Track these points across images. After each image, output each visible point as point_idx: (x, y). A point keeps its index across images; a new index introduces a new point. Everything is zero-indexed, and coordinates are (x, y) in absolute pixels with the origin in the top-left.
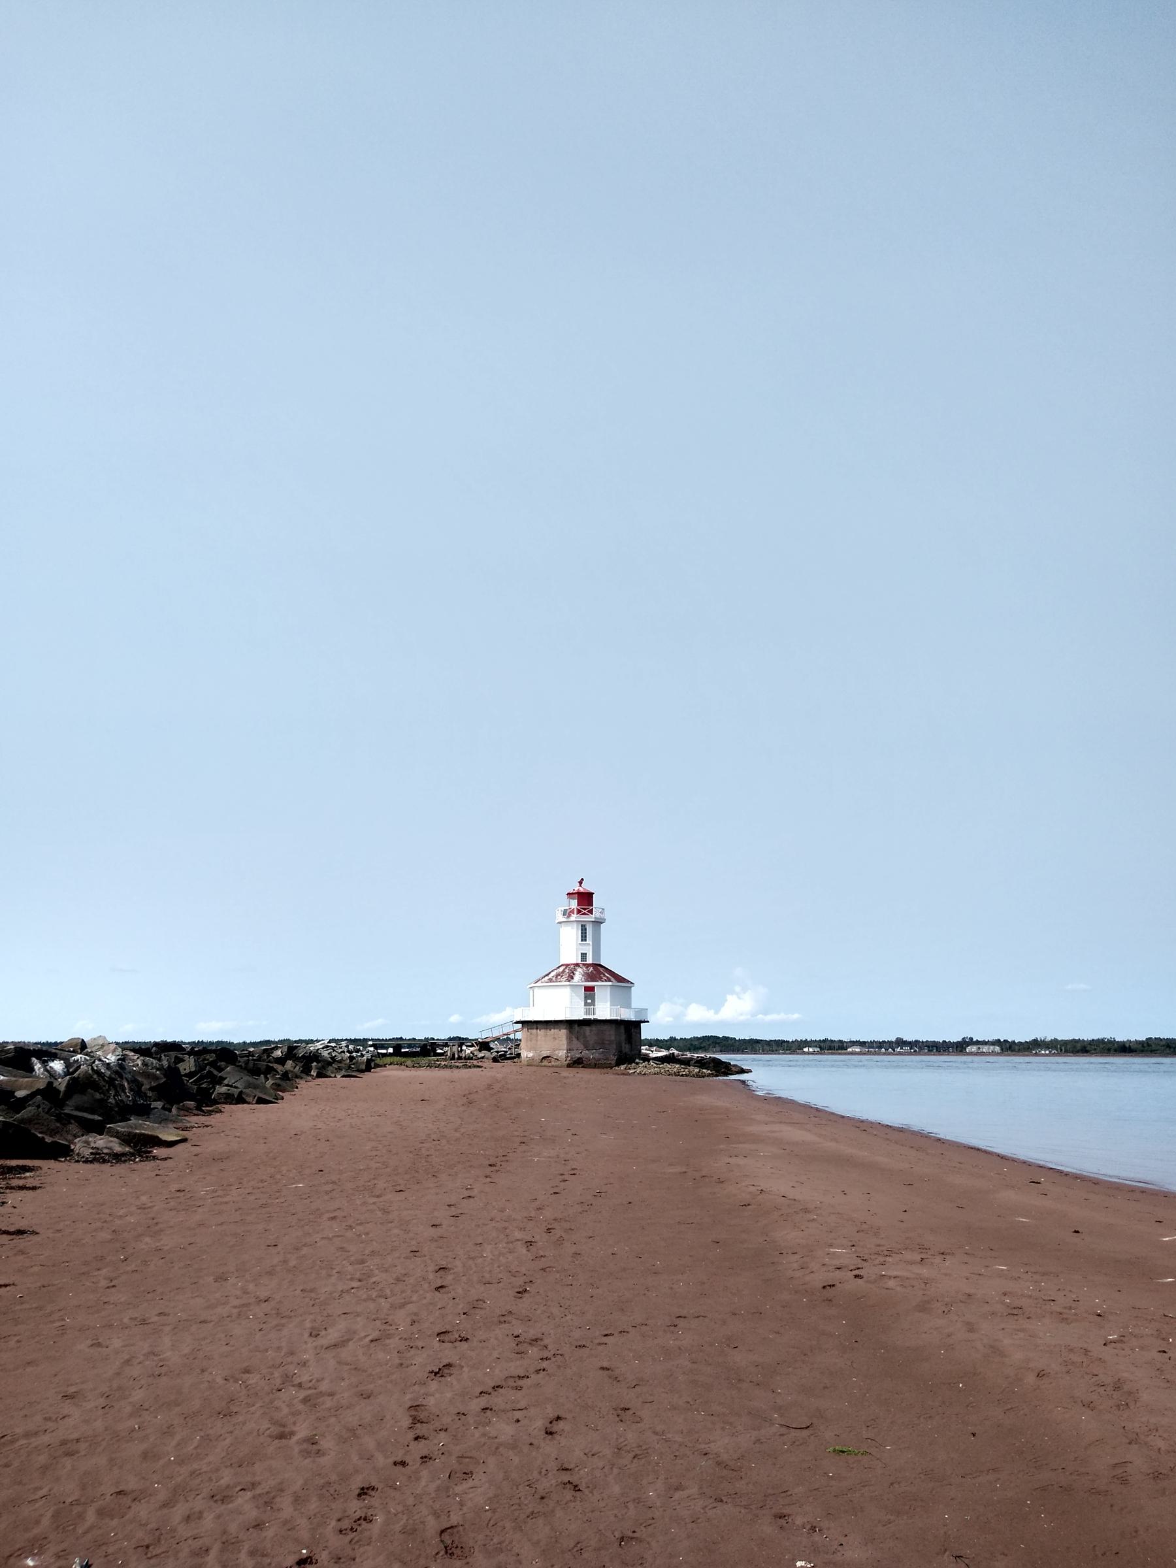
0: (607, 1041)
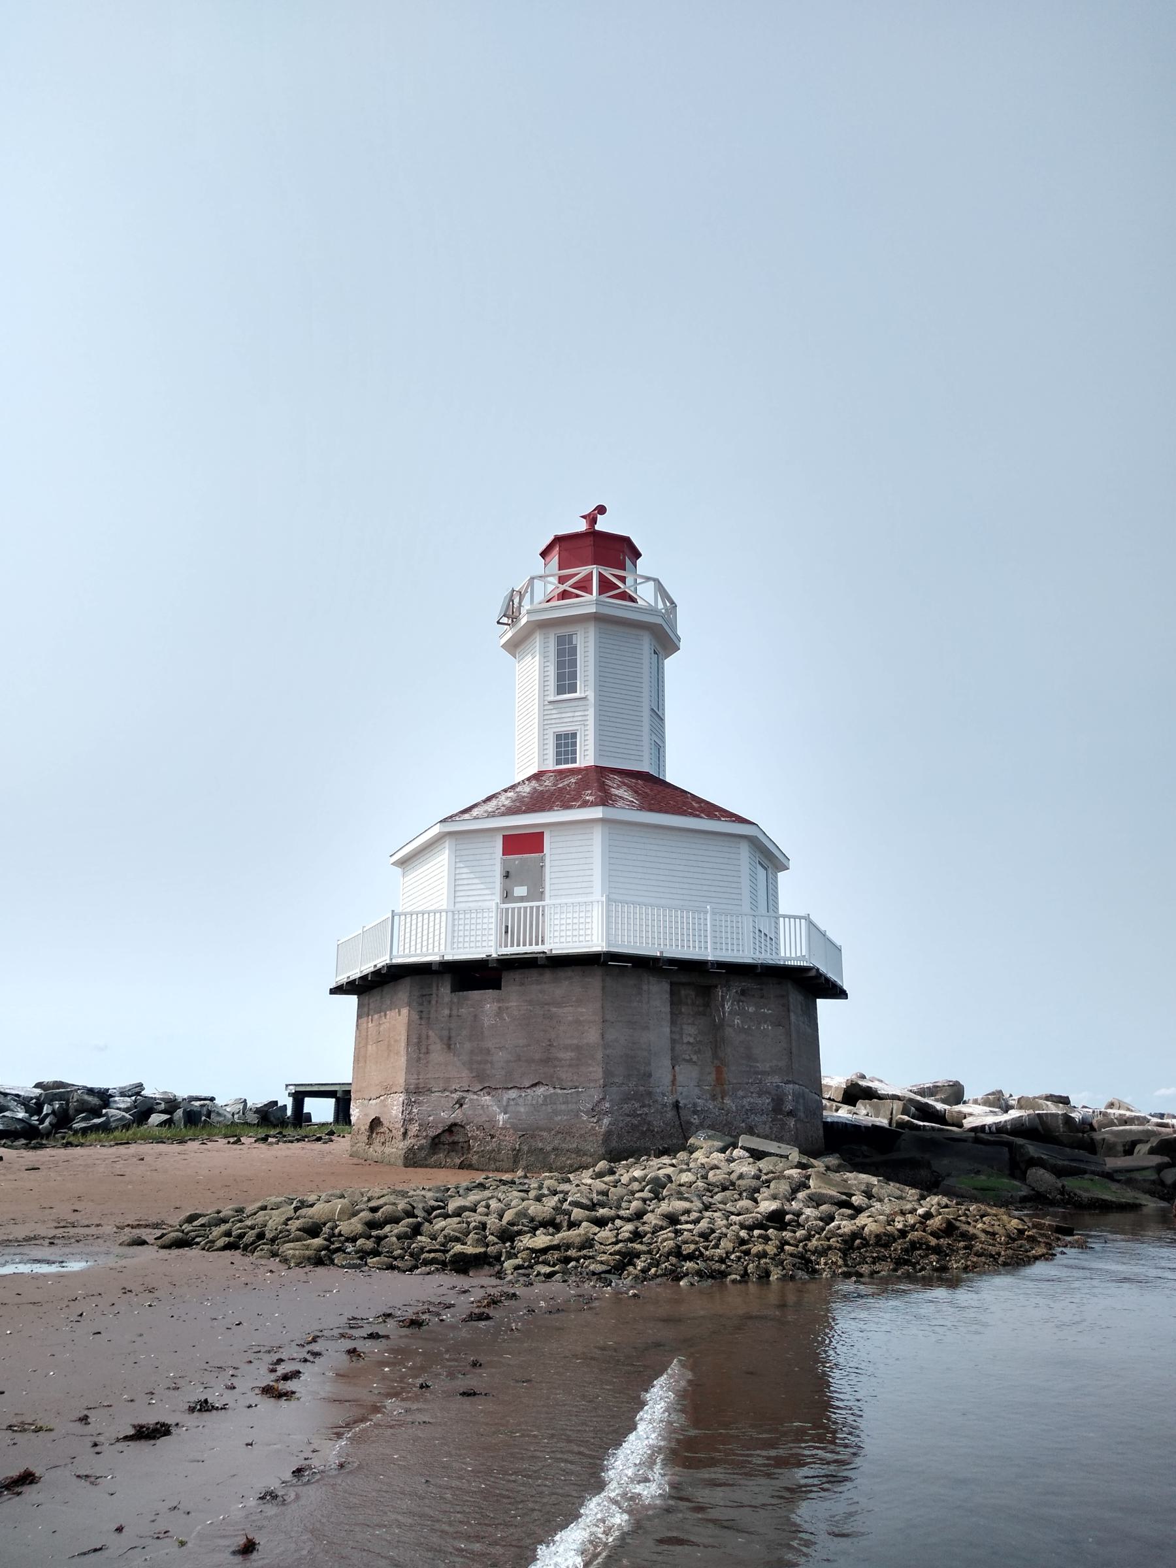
0: (566, 1048)
